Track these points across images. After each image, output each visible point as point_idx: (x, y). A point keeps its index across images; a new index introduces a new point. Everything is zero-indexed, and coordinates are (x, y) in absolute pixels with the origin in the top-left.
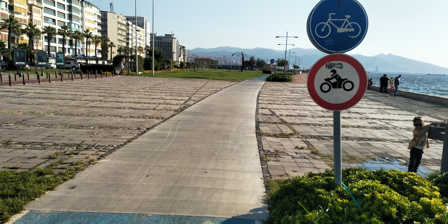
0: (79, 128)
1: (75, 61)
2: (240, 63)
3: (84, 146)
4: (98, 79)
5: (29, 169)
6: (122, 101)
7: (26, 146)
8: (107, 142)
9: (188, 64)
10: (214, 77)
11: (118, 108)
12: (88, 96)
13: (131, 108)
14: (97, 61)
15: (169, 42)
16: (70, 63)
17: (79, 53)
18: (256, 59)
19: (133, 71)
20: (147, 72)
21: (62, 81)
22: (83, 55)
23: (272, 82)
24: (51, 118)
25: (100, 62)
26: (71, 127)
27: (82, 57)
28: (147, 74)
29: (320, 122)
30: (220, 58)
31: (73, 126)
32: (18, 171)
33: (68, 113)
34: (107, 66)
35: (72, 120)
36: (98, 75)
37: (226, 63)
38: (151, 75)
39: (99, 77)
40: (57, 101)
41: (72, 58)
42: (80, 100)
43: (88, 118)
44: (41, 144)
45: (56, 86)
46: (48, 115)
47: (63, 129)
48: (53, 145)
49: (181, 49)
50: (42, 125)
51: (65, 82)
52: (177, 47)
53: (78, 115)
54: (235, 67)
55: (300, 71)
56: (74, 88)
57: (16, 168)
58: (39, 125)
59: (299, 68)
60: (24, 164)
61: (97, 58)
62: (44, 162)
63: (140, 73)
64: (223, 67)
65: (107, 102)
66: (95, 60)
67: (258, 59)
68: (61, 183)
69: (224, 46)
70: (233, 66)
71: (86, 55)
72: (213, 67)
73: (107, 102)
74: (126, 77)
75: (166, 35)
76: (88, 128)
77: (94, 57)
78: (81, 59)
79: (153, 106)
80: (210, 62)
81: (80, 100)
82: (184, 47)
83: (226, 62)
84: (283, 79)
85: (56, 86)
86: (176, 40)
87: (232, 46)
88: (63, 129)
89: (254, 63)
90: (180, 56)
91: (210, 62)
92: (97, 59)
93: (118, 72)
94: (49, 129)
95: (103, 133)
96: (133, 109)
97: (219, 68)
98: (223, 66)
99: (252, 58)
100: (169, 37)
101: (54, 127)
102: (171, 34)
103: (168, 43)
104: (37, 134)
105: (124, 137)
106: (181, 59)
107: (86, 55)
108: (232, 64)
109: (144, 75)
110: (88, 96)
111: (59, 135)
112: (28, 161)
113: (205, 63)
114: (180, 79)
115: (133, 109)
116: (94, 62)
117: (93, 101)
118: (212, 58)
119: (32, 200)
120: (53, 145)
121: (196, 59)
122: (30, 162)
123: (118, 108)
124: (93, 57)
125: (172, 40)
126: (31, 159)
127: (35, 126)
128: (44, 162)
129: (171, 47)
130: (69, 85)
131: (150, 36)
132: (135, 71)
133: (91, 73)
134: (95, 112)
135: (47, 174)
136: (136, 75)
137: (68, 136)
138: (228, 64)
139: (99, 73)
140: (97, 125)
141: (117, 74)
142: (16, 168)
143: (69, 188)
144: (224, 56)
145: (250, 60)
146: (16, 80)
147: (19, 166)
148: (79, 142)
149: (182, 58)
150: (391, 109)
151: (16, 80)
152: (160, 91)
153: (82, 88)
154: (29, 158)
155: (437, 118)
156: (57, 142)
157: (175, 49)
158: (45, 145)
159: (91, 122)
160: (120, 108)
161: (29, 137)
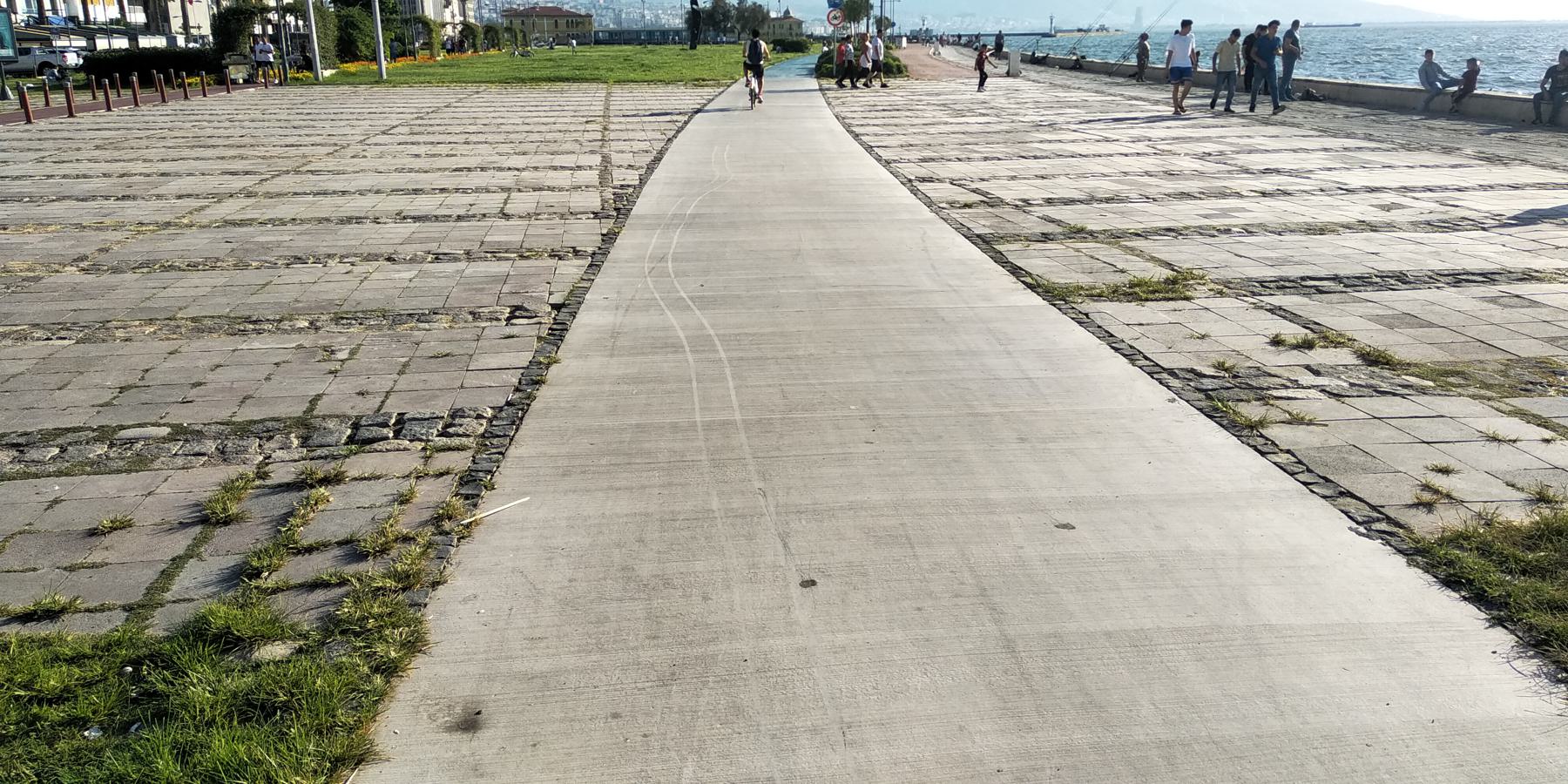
0: (244, 332)
1: (46, 41)
2: (678, 22)
3: (331, 424)
4: (172, 105)
5: (128, 608)
6: (339, 186)
7: (33, 454)
8: (435, 393)
9: (490, 30)
11: (349, 220)
12: (178, 175)
13: (402, 217)
14: (133, 39)
16: (27, 52)
17: (54, 10)
19: (300, 68)
20: (351, 67)
21: (109, 109)
22: (73, 19)
24: (75, 291)
25: (145, 42)
26: (200, 327)
27: (71, 25)
28: (353, 74)
29: (1206, 217)
31: (208, 322)
32: (75, 631)
33: (140, 259)
34: (187, 53)
35: (179, 292)
36: (142, 94)
38: (378, 80)
39: (175, 98)
40: (57, 209)
41: (31, 31)
42: (159, 197)
43: (251, 277)
44: (104, 434)
45: (15, 144)
46: (55, 278)
47: (171, 345)
48: (171, 438)
50: (58, 329)
51: (42, 124)
53: (193, 266)
54: (656, 37)
56: (97, 147)
57: (51, 614)
58: (39, 333)
59: (893, 25)
60: (84, 574)
61: (127, 24)
62: (191, 553)
63: (328, 73)
65: (279, 195)
66: (122, 33)
68: (382, 695)
70: (650, 33)
71: (82, 18)
73: (279, 195)
74: (280, 90)
76: (286, 325)
77: (117, 22)
78: (64, 32)
79: (492, 202)
80: (562, 22)
81: (159, 197)
83: (618, 20)
85: (15, 144)
88: (171, 345)
91: (562, 22)
92: (132, 32)
93: (237, 73)
94: (92, 350)
95: (378, 348)
96: (416, 219)
97: (598, 42)
98: (611, 33)
101: (120, 333)
104: (54, 380)
105: (494, 362)
106: (453, 16)
107: (82, 18)
110: (178, 175)
111: (174, 378)
112: (96, 557)
114: (494, 88)
116: (121, 43)
117: (219, 198)
120: (171, 438)
122: (111, 557)
123: (349, 220)
124: (112, 21)
126: (107, 540)
127: (23, 337)
128: (191, 553)
130: (66, 134)
132: (308, 65)
133: (113, 85)
134: (266, 247)
135: (267, 639)
136: (317, 81)
137: (222, 376)
138: (625, 26)
139: (147, 82)
140: (321, 307)
141: (234, 82)
142: (51, 614)
143: (451, 729)
146: (47, 104)
147: (63, 599)
148: (297, 410)
149: (456, 11)
150: (1373, 150)
151: (47, 104)
152: (462, 138)
153: (134, 143)
154: (93, 533)
155: (55, 221)
156: (184, 416)
158: (132, 441)
159: (287, 295)
160: (359, 220)
161: (28, 399)
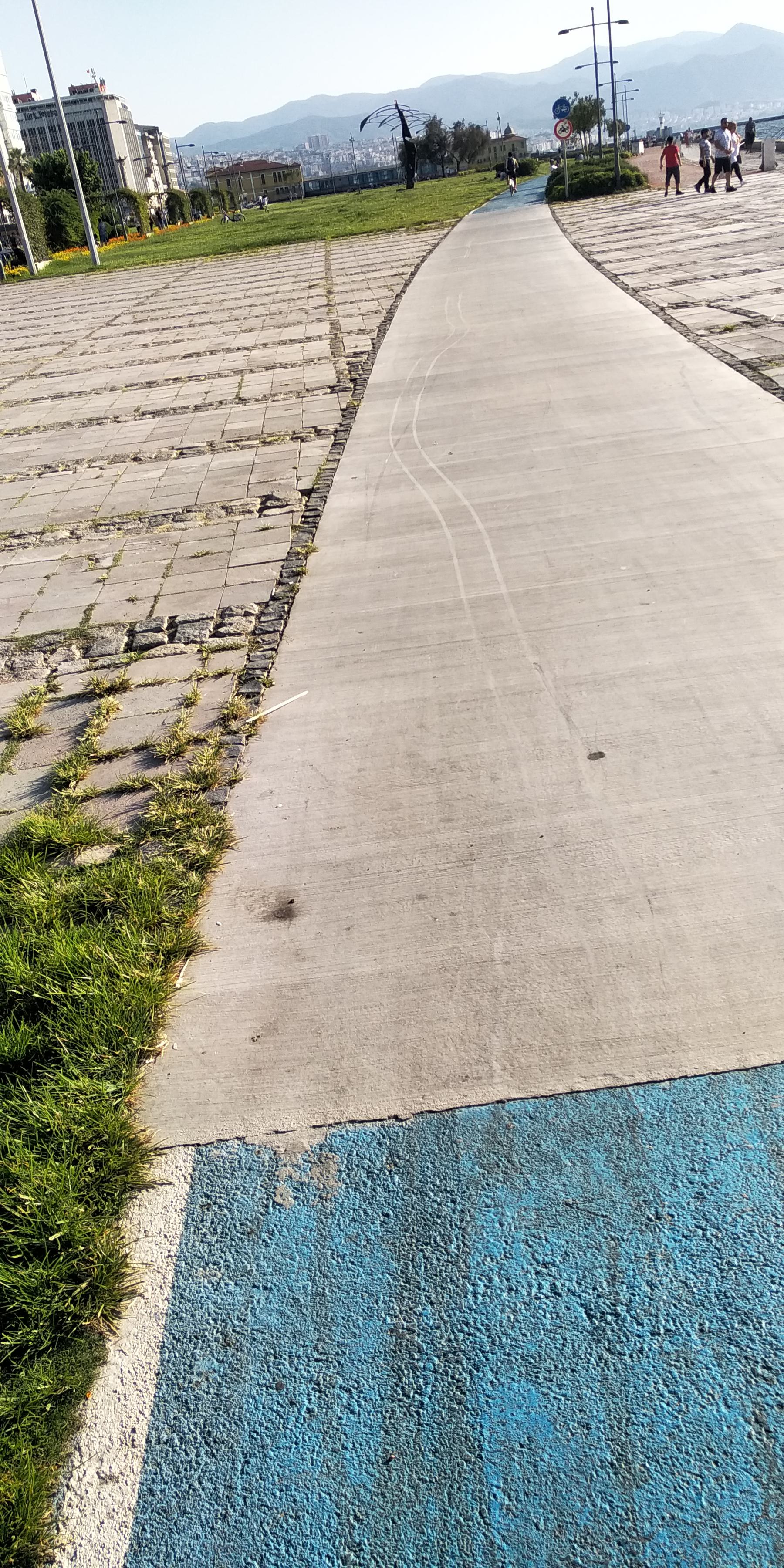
2: (388, 158)
6: (74, 387)
9: (196, 195)
10: (340, 229)
15: (92, 116)
18: (447, 125)
19: (15, 264)
20: (65, 256)
23: (575, 203)
28: (67, 264)
30: (300, 151)
37: (330, 169)
49: (144, 138)
52: (129, 136)
55: (636, 141)
64: (329, 186)
67: (457, 125)
69: (304, 96)
70: (363, 176)
72: (280, 196)
75: (73, 90)
76: (48, 537)
80: (268, 176)
82: (154, 130)
83: (327, 166)
84: (613, 180)
86: (118, 104)
87: (335, 90)
89: (443, 144)
90: (149, 172)
91: (268, 176)
96: (155, 414)
97: (309, 194)
99: (433, 125)
100: (87, 96)
102: (90, 81)
103: (91, 123)
108: (351, 170)
109: (59, 270)
113: (252, 180)
114: (209, 261)
115: (155, 414)
118: (271, 159)
119: (143, 1055)
121: (214, 174)
125: (103, 109)
129: (106, 137)
131: (14, 107)
132: (21, 259)
143: (267, 918)
144: (315, 142)
145: (428, 137)
157: (121, 145)
